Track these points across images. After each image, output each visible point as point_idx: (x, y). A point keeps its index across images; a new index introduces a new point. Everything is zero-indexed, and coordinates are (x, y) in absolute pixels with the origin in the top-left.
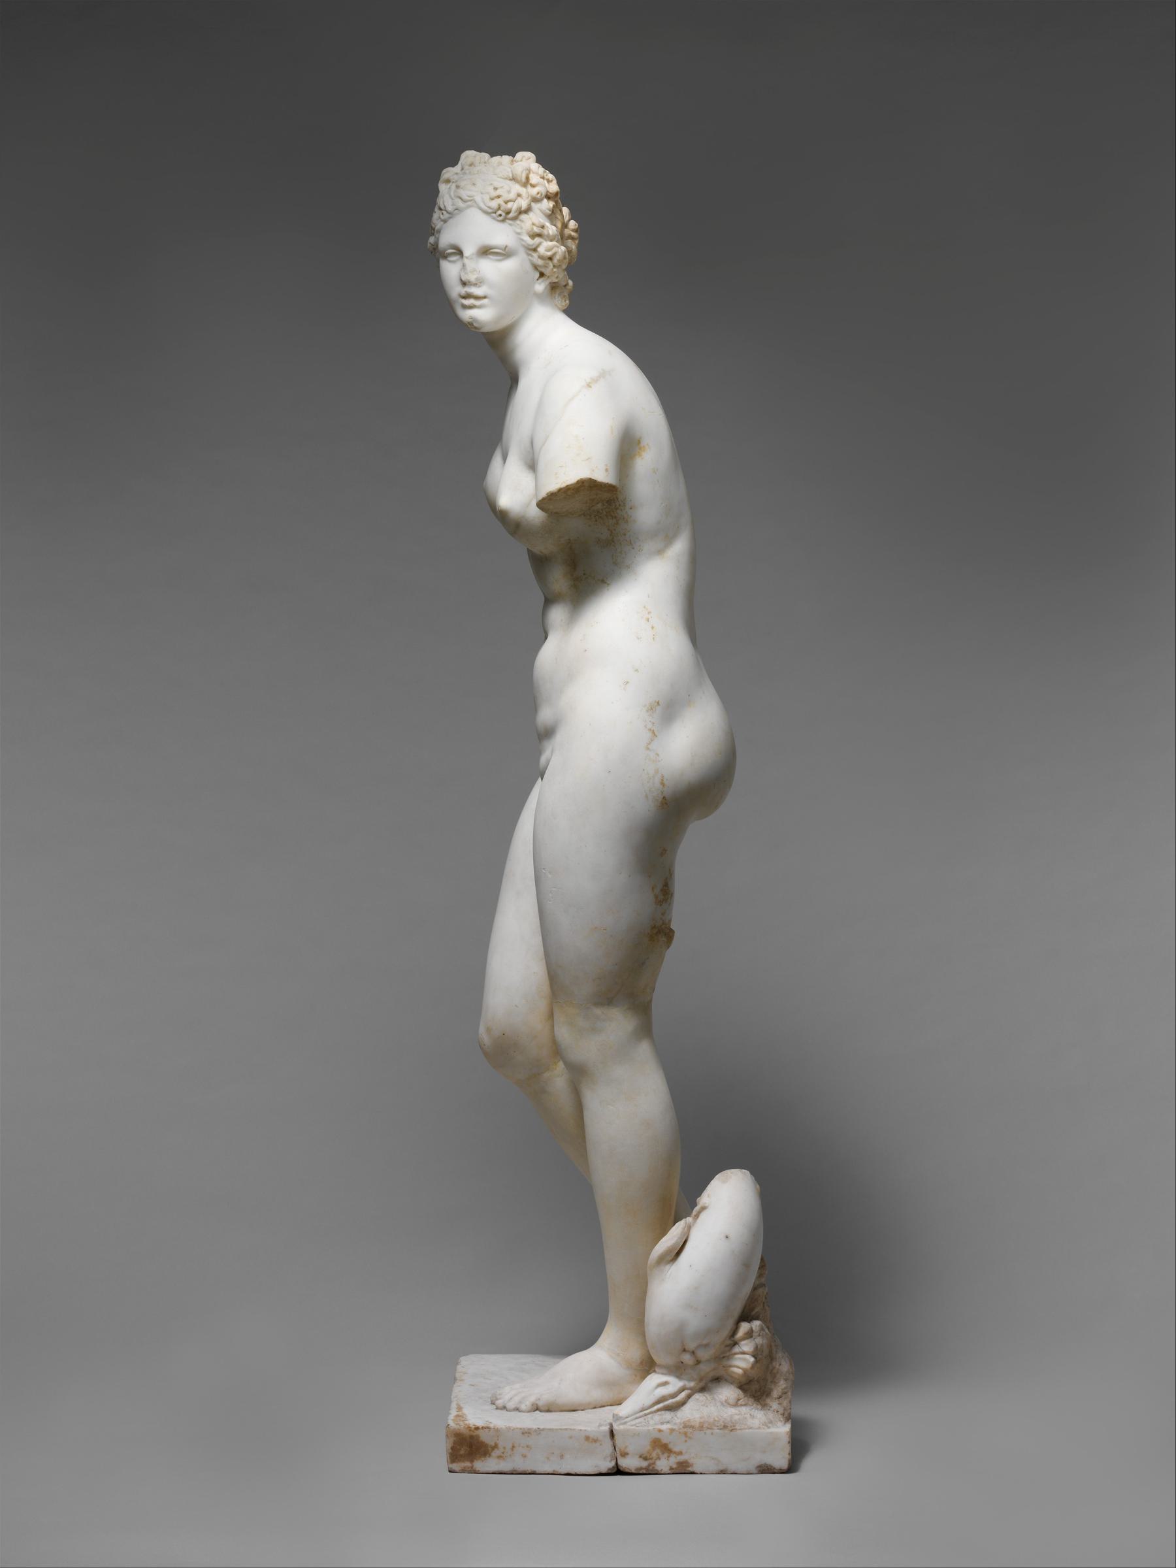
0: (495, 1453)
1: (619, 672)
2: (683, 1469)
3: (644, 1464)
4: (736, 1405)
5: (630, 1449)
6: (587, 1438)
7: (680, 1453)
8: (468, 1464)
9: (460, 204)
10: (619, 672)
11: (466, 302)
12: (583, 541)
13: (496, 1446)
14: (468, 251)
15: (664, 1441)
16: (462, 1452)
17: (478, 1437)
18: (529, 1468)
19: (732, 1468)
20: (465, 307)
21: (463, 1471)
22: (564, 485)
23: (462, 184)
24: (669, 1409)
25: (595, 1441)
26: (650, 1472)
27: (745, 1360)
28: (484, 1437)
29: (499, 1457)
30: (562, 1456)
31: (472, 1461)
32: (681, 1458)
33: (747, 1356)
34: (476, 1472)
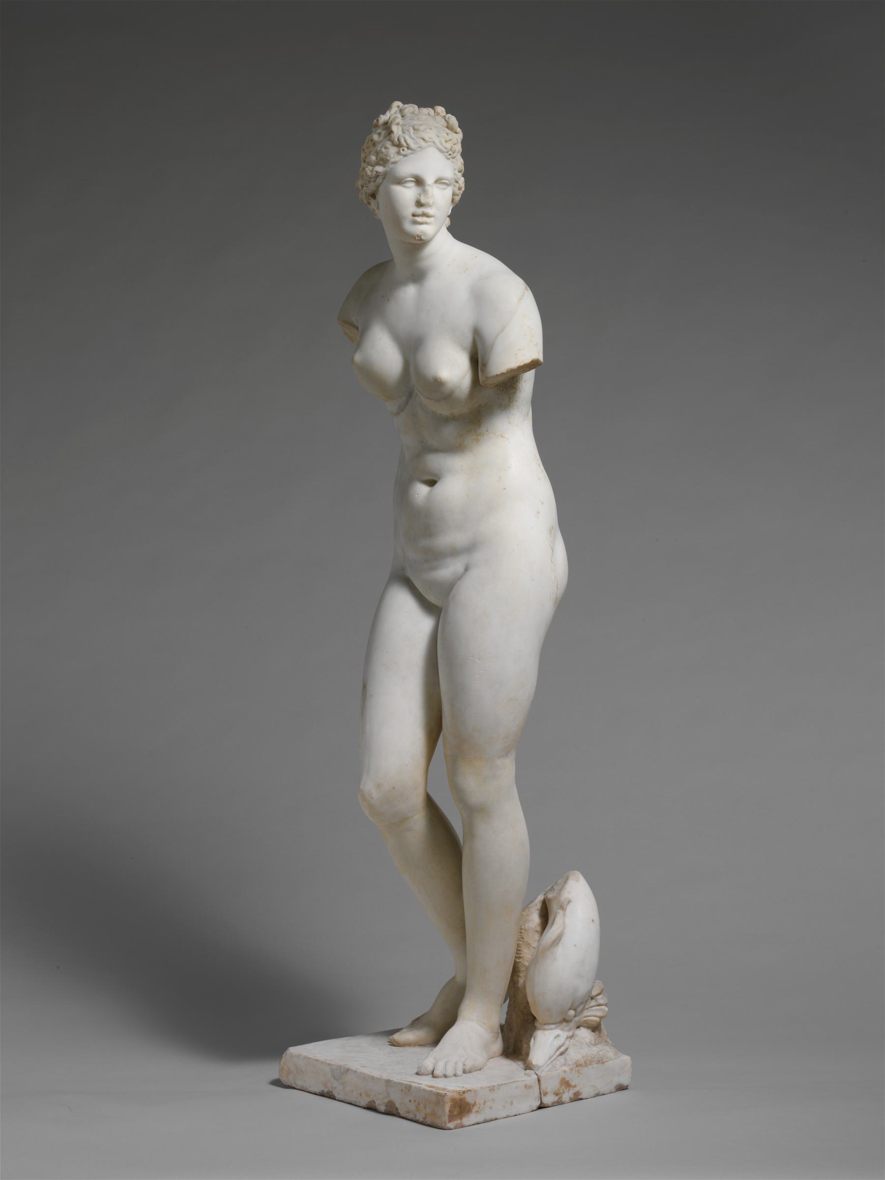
0: (475, 1109)
1: (507, 492)
2: (577, 1098)
3: (556, 1098)
4: (596, 1044)
5: (549, 1090)
6: (526, 1086)
7: (575, 1086)
8: (459, 1121)
9: (423, 144)
10: (507, 492)
11: (419, 219)
12: (491, 391)
13: (475, 1104)
14: (430, 180)
15: (567, 1079)
16: (455, 1113)
17: (465, 1098)
18: (493, 1117)
19: (602, 1091)
20: (415, 223)
21: (456, 1128)
22: (522, 364)
23: (422, 128)
24: (562, 1054)
25: (530, 1087)
26: (559, 1103)
27: (601, 1010)
28: (469, 1098)
29: (477, 1112)
30: (512, 1103)
31: (461, 1119)
32: (576, 1090)
33: (603, 1007)
34: (463, 1127)
